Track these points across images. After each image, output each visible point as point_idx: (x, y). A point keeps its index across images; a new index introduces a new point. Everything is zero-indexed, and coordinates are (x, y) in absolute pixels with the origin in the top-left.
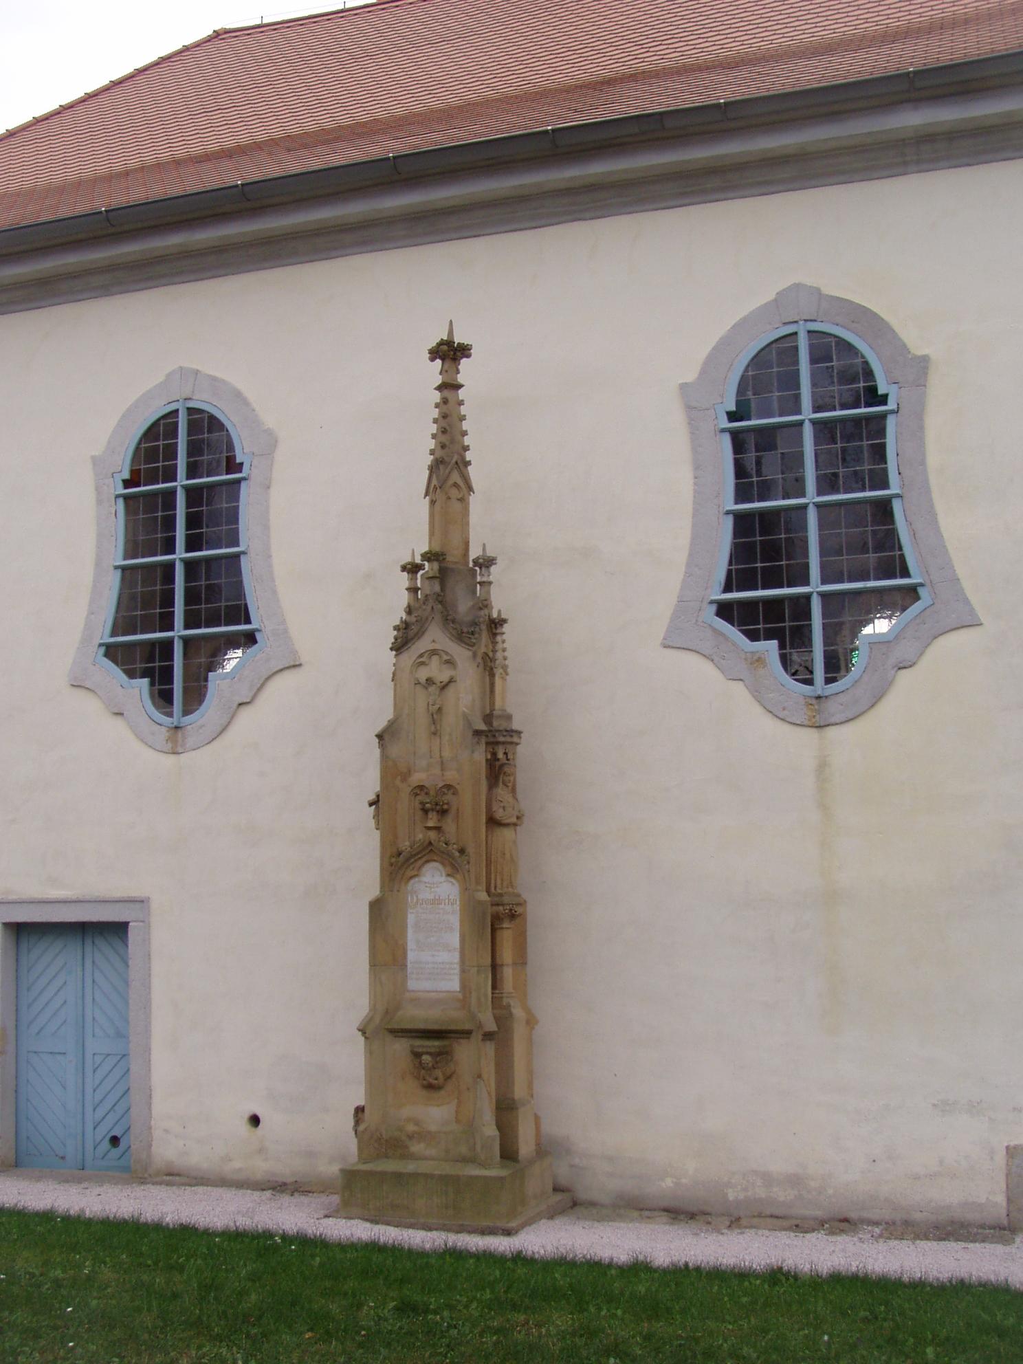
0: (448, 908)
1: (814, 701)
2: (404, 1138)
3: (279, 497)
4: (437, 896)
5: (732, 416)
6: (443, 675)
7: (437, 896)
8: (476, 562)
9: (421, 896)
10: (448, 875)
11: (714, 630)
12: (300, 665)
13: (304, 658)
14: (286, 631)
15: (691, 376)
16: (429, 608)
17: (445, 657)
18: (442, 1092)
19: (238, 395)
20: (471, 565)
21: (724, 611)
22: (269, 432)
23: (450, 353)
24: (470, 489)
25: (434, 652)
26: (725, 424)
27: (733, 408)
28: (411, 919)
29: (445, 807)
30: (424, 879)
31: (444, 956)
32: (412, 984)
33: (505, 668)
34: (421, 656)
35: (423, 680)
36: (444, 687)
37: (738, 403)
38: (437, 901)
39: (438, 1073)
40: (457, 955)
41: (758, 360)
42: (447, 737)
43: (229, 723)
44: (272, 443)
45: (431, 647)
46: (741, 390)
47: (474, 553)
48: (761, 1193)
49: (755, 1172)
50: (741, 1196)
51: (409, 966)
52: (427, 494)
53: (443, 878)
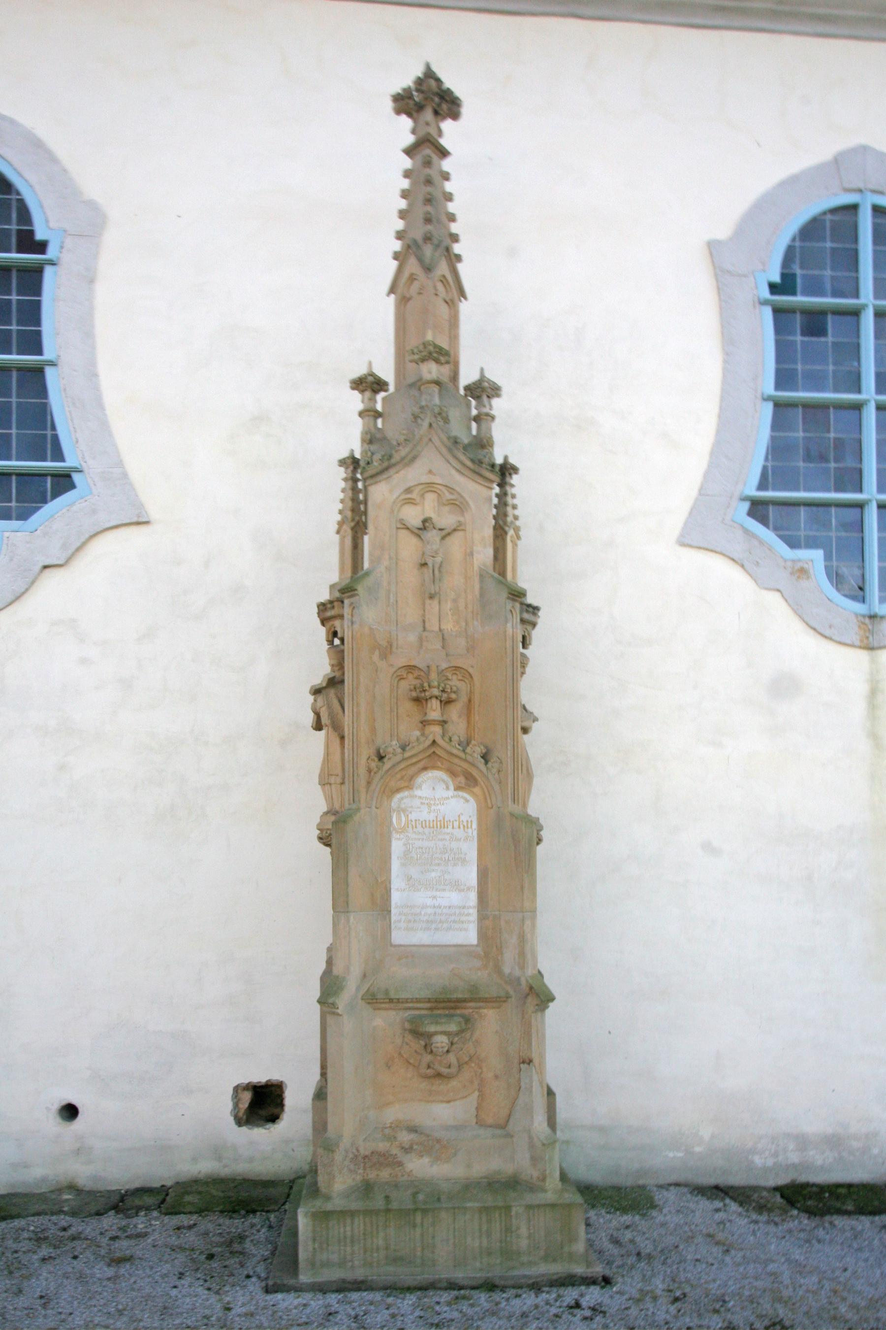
0: (459, 833)
1: (867, 621)
2: (394, 1151)
3: (107, 295)
4: (436, 813)
5: (774, 288)
6: (447, 520)
7: (436, 813)
8: (467, 388)
9: (413, 816)
10: (458, 788)
11: (746, 531)
12: (147, 523)
13: (153, 512)
14: (125, 475)
15: (723, 232)
16: (426, 424)
17: (448, 496)
18: (454, 1083)
19: (38, 144)
20: (462, 392)
21: (758, 509)
22: (92, 205)
23: (429, 101)
24: (462, 293)
25: (430, 487)
26: (766, 293)
27: (776, 278)
28: (397, 846)
29: (453, 696)
30: (418, 793)
31: (453, 898)
32: (398, 937)
33: (517, 530)
34: (408, 490)
35: (416, 522)
36: (446, 534)
37: (783, 276)
38: (441, 824)
39: (452, 1058)
40: (472, 898)
41: (811, 230)
42: (449, 605)
43: (27, 590)
44: (94, 223)
45: (425, 479)
46: (789, 256)
47: (467, 376)
48: (794, 1158)
49: (788, 1135)
50: (770, 1162)
51: (393, 911)
52: (392, 290)
53: (451, 792)
